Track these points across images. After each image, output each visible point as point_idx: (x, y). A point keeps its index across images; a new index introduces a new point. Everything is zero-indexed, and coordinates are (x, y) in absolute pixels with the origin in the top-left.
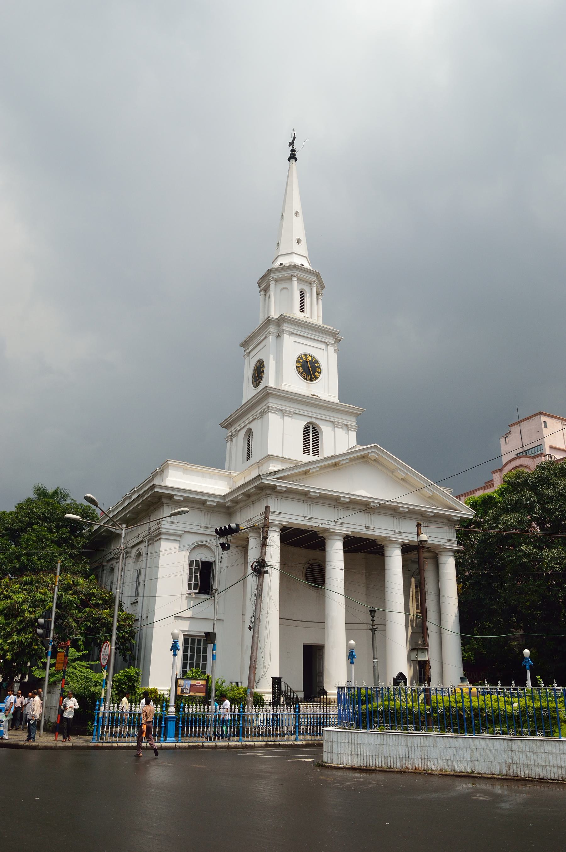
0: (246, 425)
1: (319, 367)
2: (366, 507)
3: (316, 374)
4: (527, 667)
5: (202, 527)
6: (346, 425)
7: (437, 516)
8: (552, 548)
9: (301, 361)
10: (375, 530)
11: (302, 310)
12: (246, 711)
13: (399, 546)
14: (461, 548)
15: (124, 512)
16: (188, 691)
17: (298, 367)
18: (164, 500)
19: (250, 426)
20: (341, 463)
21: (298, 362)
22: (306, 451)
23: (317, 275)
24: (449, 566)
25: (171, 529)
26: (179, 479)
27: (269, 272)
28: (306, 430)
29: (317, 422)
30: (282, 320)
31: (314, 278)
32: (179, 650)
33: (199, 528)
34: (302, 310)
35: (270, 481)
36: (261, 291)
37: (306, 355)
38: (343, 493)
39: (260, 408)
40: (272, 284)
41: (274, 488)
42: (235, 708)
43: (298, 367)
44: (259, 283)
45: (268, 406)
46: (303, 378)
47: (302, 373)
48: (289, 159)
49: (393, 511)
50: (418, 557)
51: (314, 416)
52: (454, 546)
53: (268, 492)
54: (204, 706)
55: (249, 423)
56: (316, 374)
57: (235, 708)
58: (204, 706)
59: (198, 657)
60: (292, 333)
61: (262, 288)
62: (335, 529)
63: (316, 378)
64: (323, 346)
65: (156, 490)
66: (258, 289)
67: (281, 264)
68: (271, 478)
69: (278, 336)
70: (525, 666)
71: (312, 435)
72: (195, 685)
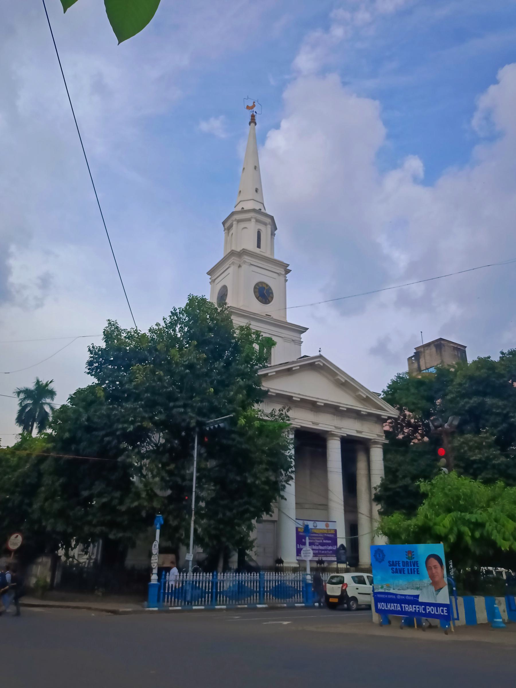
1: (272, 293)
2: (312, 406)
6: (293, 340)
7: (370, 415)
8: (153, 451)
10: (320, 425)
11: (259, 246)
12: (219, 578)
13: (339, 439)
14: (387, 442)
15: (285, 366)
20: (269, 375)
21: (255, 288)
23: (272, 218)
24: (377, 454)
27: (233, 214)
30: (244, 252)
31: (268, 220)
32: (417, 596)
34: (259, 246)
36: (225, 229)
38: (295, 393)
44: (224, 223)
48: (250, 124)
49: (334, 410)
50: (352, 447)
52: (383, 440)
60: (251, 264)
61: (226, 228)
64: (275, 275)
66: (223, 228)
67: (243, 208)
69: (240, 266)
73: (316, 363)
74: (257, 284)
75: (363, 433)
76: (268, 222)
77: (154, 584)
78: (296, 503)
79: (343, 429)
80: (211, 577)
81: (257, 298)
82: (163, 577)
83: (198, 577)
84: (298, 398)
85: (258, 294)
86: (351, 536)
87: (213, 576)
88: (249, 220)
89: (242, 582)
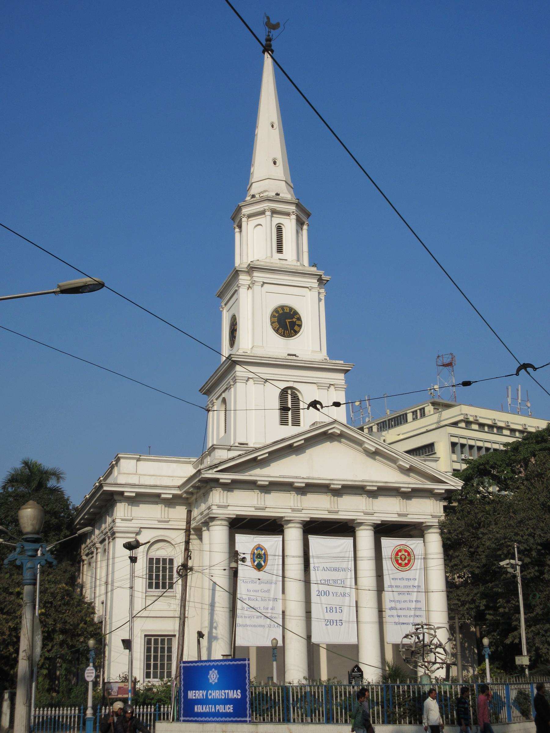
0: (221, 395)
3: (296, 328)
4: (487, 656)
5: (159, 521)
9: (277, 315)
10: (340, 513)
16: (116, 694)
17: (272, 323)
18: (116, 497)
19: (223, 395)
21: (272, 316)
22: (284, 421)
25: (126, 527)
26: (131, 473)
28: (284, 393)
29: (296, 385)
33: (156, 522)
34: (280, 250)
35: (210, 474)
37: (282, 307)
38: (297, 478)
39: (229, 379)
40: (244, 219)
41: (217, 480)
42: (151, 708)
43: (273, 322)
45: (235, 377)
46: (280, 335)
47: (278, 329)
51: (289, 377)
53: (212, 484)
54: (48, 709)
55: (224, 392)
56: (296, 328)
57: (151, 708)
58: (48, 709)
59: (162, 657)
62: (290, 517)
63: (296, 333)
65: (105, 488)
68: (210, 471)
70: (484, 655)
71: (289, 406)
72: (123, 687)
73: (330, 432)
74: (276, 310)
75: (409, 516)
76: (291, 211)
77: (89, 718)
78: (311, 612)
79: (375, 515)
80: (77, 712)
81: (277, 331)
82: (98, 711)
83: (69, 712)
84: (303, 483)
85: (276, 325)
86: (245, 665)
87: (80, 710)
88: (263, 213)
89: (59, 717)
